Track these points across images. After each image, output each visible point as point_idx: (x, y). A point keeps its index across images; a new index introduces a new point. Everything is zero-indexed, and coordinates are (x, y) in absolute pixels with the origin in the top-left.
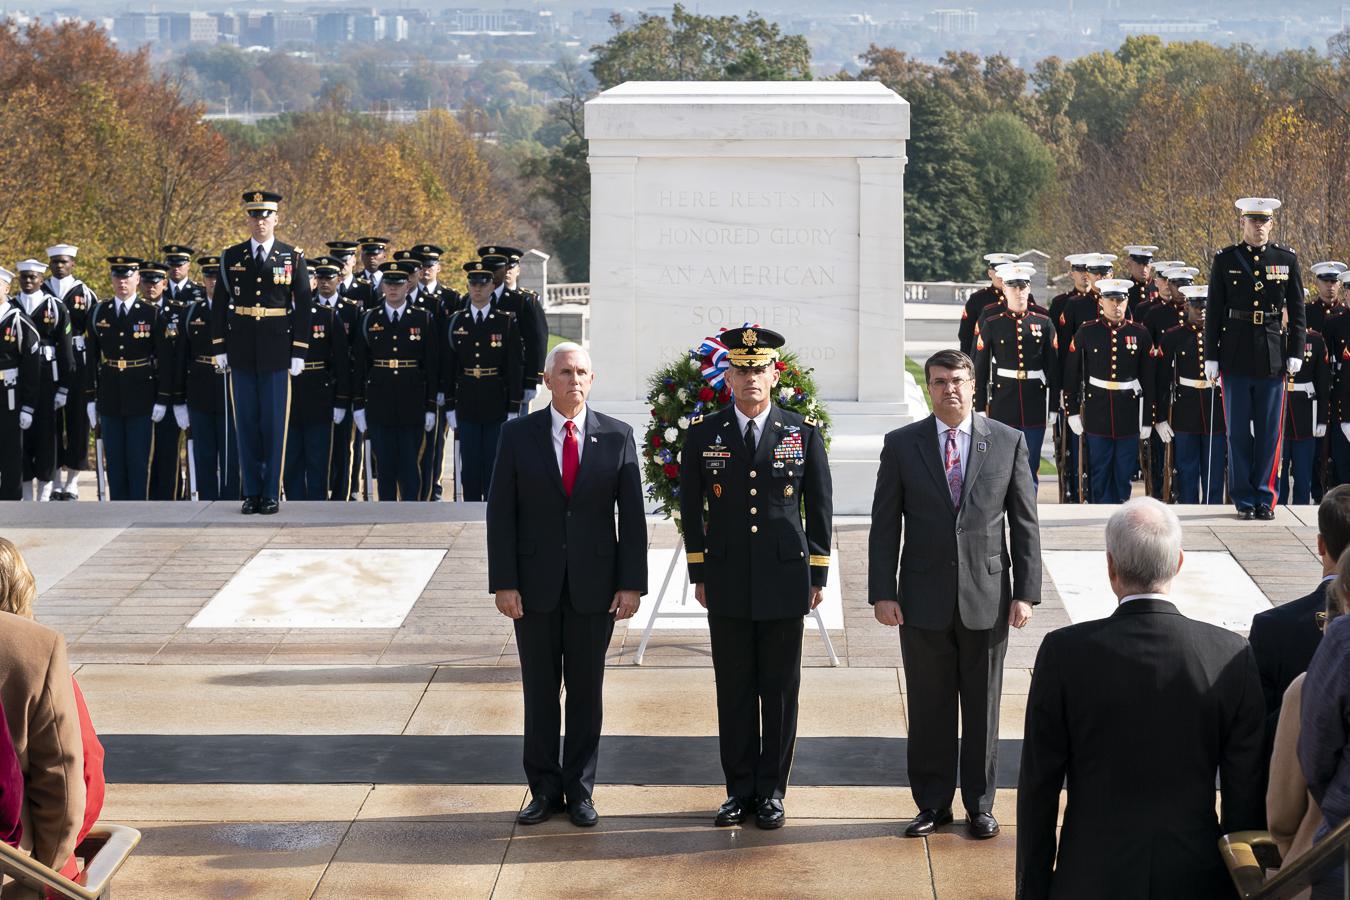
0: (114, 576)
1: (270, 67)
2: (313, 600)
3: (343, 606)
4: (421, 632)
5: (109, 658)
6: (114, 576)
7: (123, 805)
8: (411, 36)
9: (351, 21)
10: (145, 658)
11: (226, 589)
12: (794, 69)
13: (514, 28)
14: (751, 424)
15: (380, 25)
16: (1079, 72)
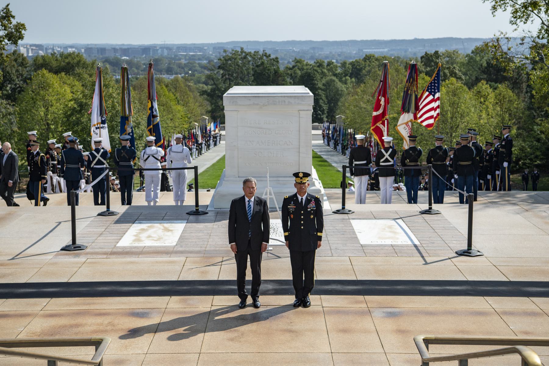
0: (95, 230)
2: (151, 237)
3: (159, 239)
4: (181, 247)
5: (95, 256)
6: (95, 230)
8: (168, 54)
9: (151, 50)
10: (105, 256)
11: (127, 234)
13: (197, 52)
14: (302, 199)
15: (160, 51)
16: (352, 64)
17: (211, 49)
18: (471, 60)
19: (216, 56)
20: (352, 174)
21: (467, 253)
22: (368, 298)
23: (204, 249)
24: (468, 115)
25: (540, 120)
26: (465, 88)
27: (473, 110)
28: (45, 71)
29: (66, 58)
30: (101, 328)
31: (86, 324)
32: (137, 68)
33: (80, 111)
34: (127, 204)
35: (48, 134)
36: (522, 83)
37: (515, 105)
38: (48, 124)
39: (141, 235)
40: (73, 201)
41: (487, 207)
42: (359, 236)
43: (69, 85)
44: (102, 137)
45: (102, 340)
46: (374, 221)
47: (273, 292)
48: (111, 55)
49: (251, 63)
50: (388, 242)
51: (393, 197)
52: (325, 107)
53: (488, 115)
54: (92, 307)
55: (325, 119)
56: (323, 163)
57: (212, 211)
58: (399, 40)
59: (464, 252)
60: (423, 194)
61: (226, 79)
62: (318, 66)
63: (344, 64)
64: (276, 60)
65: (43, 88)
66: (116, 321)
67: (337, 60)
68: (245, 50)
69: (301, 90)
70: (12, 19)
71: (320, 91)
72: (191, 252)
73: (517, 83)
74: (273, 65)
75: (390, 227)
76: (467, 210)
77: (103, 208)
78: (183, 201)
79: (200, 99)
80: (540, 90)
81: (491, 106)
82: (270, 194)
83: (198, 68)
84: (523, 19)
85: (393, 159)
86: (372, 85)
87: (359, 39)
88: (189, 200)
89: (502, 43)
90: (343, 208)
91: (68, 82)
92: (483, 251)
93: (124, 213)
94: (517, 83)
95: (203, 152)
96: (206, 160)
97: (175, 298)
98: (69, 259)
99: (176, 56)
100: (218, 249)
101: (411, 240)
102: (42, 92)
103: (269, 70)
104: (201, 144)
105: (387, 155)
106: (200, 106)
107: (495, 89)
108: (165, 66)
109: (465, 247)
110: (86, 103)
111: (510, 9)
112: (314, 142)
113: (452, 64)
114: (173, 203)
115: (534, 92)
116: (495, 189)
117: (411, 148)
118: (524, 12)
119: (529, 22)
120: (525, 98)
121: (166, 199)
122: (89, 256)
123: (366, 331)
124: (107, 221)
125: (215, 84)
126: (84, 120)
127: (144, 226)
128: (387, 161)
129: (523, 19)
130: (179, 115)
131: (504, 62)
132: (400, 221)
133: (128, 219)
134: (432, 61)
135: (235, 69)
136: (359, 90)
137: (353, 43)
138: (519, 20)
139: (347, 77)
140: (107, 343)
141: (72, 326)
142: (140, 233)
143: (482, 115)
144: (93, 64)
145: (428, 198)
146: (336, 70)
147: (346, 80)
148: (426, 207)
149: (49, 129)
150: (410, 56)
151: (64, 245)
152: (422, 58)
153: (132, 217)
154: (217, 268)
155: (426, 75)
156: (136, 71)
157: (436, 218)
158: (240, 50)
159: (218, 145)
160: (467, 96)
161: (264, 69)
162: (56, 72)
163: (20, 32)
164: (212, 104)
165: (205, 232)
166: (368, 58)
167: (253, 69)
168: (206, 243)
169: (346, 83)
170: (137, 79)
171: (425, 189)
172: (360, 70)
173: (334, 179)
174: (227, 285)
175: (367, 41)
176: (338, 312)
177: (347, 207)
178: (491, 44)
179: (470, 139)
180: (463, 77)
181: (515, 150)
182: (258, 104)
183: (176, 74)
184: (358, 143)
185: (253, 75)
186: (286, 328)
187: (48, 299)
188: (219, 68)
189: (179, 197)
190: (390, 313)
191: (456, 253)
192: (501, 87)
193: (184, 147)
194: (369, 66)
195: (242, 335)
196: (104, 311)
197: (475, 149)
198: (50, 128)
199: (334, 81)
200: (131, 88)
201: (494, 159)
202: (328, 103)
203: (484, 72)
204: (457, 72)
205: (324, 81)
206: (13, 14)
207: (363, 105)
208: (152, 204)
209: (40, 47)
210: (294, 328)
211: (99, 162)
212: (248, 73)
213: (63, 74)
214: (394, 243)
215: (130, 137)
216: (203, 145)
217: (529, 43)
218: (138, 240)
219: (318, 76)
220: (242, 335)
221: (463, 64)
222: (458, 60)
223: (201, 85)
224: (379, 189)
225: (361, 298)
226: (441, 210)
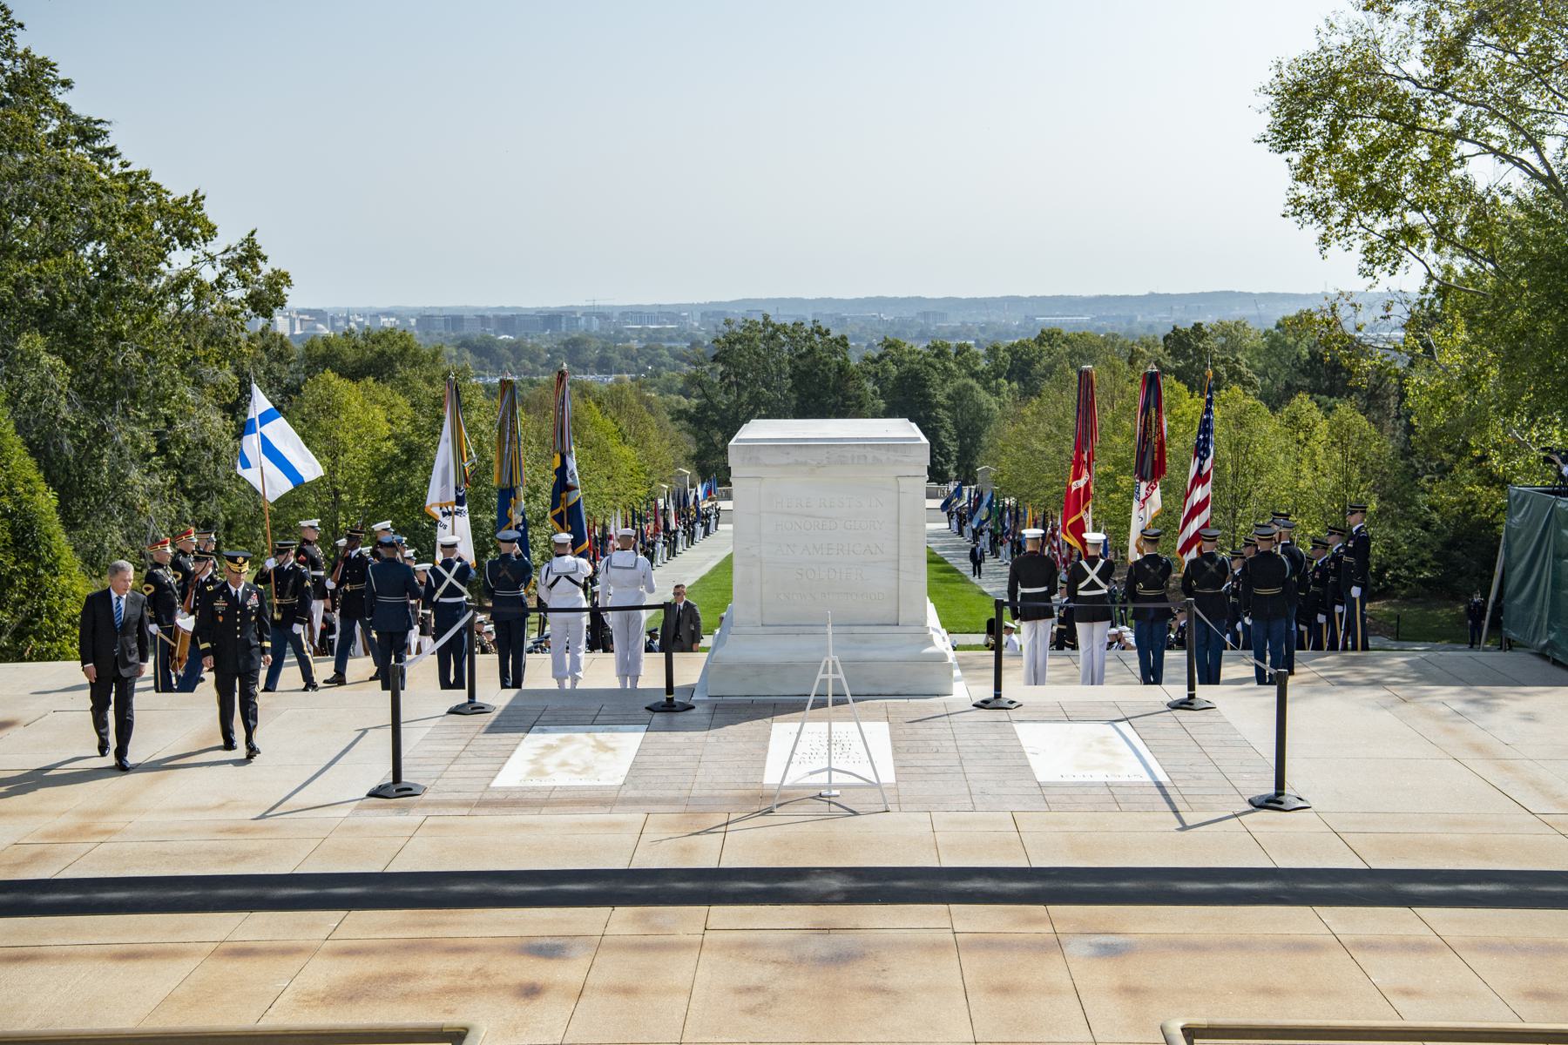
1: (516, 349)
3: (587, 769)
4: (636, 788)
7: (840, 956)
10: (466, 811)
11: (513, 756)
12: (221, 378)
15: (582, 322)
16: (1011, 349)
17: (697, 315)
18: (1274, 345)
19: (707, 333)
20: (1015, 616)
21: (1273, 802)
22: (1055, 910)
23: (686, 793)
24: (1271, 468)
25: (1429, 481)
26: (1265, 409)
27: (1281, 458)
28: (330, 375)
29: (376, 341)
30: (460, 982)
31: (425, 974)
32: (531, 360)
33: (408, 462)
34: (514, 687)
35: (336, 514)
36: (1388, 397)
37: (1373, 449)
38: (337, 493)
39: (545, 761)
40: (390, 678)
41: (1315, 691)
42: (1034, 762)
43: (383, 403)
44: (457, 534)
45: (467, 1030)
46: (1068, 726)
47: (842, 897)
48: (474, 332)
49: (786, 349)
50: (1099, 776)
51: (1108, 665)
52: (953, 447)
53: (1316, 469)
54: (439, 932)
55: (953, 474)
56: (948, 575)
57: (703, 702)
58: (1115, 297)
59: (1268, 801)
60: (1175, 659)
61: (731, 384)
62: (937, 356)
63: (993, 352)
64: (842, 342)
65: (327, 412)
66: (492, 967)
67: (977, 341)
68: (773, 320)
69: (903, 429)
70: (261, 264)
71: (940, 411)
72: (658, 801)
73: (1378, 397)
74: (835, 353)
75: (1103, 741)
76: (1275, 699)
77: (461, 696)
78: (636, 678)
79: (672, 428)
80: (1429, 419)
81: (1320, 449)
82: (835, 671)
83: (668, 359)
84: (1388, 265)
85: (1106, 582)
86: (1061, 402)
87: (1026, 293)
88: (651, 673)
89: (1344, 312)
90: (997, 696)
91: (382, 397)
92: (1310, 799)
93: (508, 708)
94: (1378, 397)
95: (679, 548)
96: (686, 568)
97: (623, 912)
98: (387, 817)
99: (619, 332)
100: (716, 793)
101: (1151, 773)
102: (323, 422)
103: (825, 364)
104: (676, 532)
105: (1093, 574)
106: (671, 446)
107: (1330, 409)
108: (593, 353)
109: (1270, 790)
110: (420, 446)
111: (1359, 245)
112: (931, 526)
113: (1234, 351)
114: (617, 685)
115: (1414, 420)
116: (1333, 647)
117: (1146, 559)
118: (1388, 249)
119: (1400, 271)
120: (1395, 429)
121: (599, 672)
122: (430, 811)
123: (1052, 991)
124: (469, 727)
125: (705, 395)
126: (415, 482)
127: (552, 738)
128: (1093, 586)
129: (1388, 265)
130: (625, 469)
131: (1350, 356)
132: (1124, 726)
133: (516, 721)
134: (1190, 345)
135: (750, 364)
136: (1026, 411)
137: (1014, 302)
138: (1378, 268)
139: (1001, 380)
140: (477, 1037)
141: (394, 978)
142: (542, 755)
143: (1300, 470)
144: (436, 354)
145: (1185, 668)
146: (976, 364)
147: (999, 386)
148: (1181, 692)
149: (337, 502)
150: (1140, 332)
151: (374, 784)
152: (1166, 338)
153: (523, 718)
154: (716, 839)
155: (1178, 379)
156: (530, 366)
157: (1204, 719)
158: (761, 320)
159: (714, 535)
160: (1269, 426)
161: (816, 363)
162: (354, 374)
163: (278, 292)
164: (698, 440)
165: (689, 752)
166: (1047, 337)
167: (790, 362)
168: (690, 779)
169: (998, 394)
170: (532, 383)
171: (1180, 644)
172: (1030, 363)
173: (974, 611)
174: (739, 880)
175: (1044, 298)
176: (987, 944)
177: (1006, 693)
178: (1318, 318)
179: (1276, 536)
180: (1258, 381)
181: (1377, 550)
182: (805, 464)
183: (620, 372)
184: (1029, 548)
185: (791, 377)
186: (871, 983)
187: (342, 913)
188: (715, 359)
189: (629, 669)
190: (1106, 946)
191: (1251, 802)
192: (1345, 409)
193: (641, 557)
194: (1050, 354)
195: (775, 999)
196: (466, 942)
197: (1290, 559)
198: (341, 501)
199: (972, 388)
200: (519, 410)
201: (1332, 579)
202: (959, 436)
203: (1302, 371)
204: (1244, 369)
205: (949, 390)
206: (263, 251)
207: (1039, 446)
208: (568, 684)
209: (319, 315)
210: (891, 982)
211: (452, 591)
212: (780, 371)
213: (370, 380)
214: (1110, 779)
215: (518, 535)
216: (680, 534)
217: (1400, 313)
218: (539, 772)
219: (937, 378)
220: (775, 999)
221: (1257, 352)
222: (1246, 342)
223: (675, 397)
224: (1075, 647)
225: (1038, 910)
226: (1216, 701)
